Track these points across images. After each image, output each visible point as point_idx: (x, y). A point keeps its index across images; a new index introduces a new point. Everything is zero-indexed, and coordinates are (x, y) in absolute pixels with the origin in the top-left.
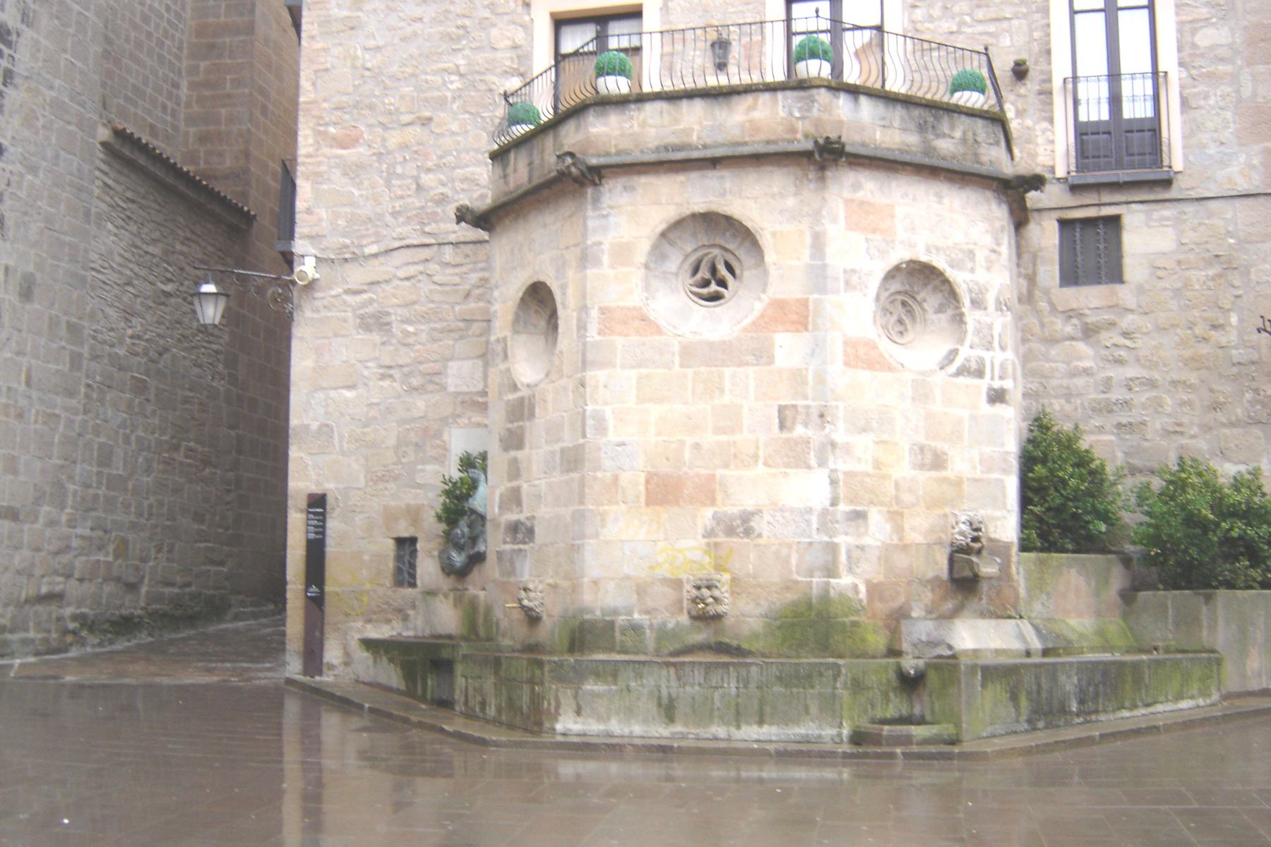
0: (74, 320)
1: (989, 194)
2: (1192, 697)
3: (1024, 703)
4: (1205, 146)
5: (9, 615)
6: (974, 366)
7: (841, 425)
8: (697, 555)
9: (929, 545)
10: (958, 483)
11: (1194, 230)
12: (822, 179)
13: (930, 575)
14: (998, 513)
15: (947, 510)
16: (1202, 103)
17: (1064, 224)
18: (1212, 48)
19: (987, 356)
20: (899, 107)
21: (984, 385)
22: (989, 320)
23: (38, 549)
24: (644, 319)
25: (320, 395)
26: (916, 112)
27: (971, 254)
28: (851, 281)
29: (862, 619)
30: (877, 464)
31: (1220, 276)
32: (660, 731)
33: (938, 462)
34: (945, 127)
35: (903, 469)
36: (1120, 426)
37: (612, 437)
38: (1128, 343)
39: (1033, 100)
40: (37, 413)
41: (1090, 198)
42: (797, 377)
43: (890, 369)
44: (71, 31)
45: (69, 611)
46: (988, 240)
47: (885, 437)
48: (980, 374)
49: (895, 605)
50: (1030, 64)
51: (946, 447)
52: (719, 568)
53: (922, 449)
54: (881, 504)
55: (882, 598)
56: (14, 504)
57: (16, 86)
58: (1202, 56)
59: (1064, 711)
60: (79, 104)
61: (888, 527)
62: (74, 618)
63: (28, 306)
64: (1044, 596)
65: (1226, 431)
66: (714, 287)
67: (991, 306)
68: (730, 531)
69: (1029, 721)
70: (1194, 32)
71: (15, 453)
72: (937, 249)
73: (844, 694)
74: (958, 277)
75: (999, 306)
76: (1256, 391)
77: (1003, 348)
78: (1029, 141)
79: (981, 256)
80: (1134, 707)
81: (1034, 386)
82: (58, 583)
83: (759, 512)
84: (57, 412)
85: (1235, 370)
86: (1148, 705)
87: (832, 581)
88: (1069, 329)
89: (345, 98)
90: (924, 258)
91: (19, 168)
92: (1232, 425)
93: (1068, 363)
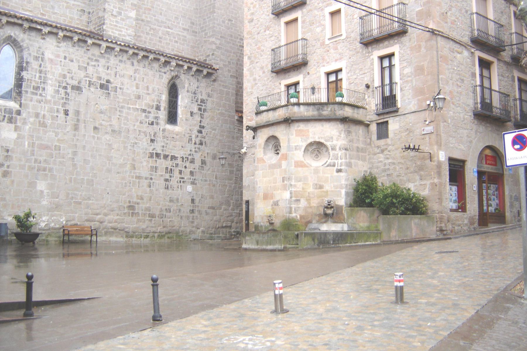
0: (230, 162)
1: (338, 122)
2: (371, 241)
3: (316, 241)
4: (405, 100)
5: (213, 231)
6: (332, 164)
7: (293, 180)
8: (270, 210)
9: (318, 207)
10: (327, 192)
11: (403, 122)
12: (289, 126)
13: (318, 213)
14: (339, 198)
15: (323, 198)
16: (405, 89)
17: (378, 124)
18: (407, 74)
19: (336, 161)
20: (312, 106)
21: (335, 168)
22: (337, 153)
23: (222, 216)
24: (263, 160)
25: (248, 178)
26: (317, 106)
27: (332, 138)
28: (297, 148)
29: (298, 223)
30: (303, 189)
31: (408, 134)
32: (256, 247)
33: (321, 187)
34: (325, 108)
35: (311, 189)
36: (387, 175)
37: (258, 186)
38: (389, 153)
39: (371, 93)
40: (219, 185)
41: (382, 117)
42: (285, 170)
43: (307, 167)
44: (224, 95)
45: (233, 230)
46: (338, 134)
47: (306, 182)
48: (334, 166)
49: (308, 220)
50: (369, 84)
51: (323, 184)
52: (273, 213)
53: (316, 185)
54: (304, 197)
55: (304, 218)
56: (213, 206)
57: (207, 112)
58: (405, 76)
59: (328, 243)
60: (228, 112)
61: (306, 203)
62: (234, 232)
63: (215, 161)
64: (353, 218)
65: (409, 175)
66: (278, 151)
67: (338, 149)
68: (275, 205)
69: (318, 245)
70: (403, 70)
71: (213, 194)
72: (322, 138)
73: (282, 239)
74: (328, 144)
75: (340, 149)
76: (416, 163)
77: (341, 159)
78: (370, 104)
79: (335, 138)
80: (351, 243)
81: (371, 166)
82: (229, 224)
83: (279, 200)
84: (226, 184)
85: (411, 158)
86: (355, 243)
87: (290, 215)
88: (378, 151)
89: (251, 110)
90: (318, 140)
91: (210, 130)
92: (411, 173)
93: (377, 159)
